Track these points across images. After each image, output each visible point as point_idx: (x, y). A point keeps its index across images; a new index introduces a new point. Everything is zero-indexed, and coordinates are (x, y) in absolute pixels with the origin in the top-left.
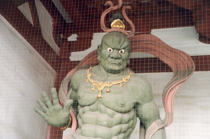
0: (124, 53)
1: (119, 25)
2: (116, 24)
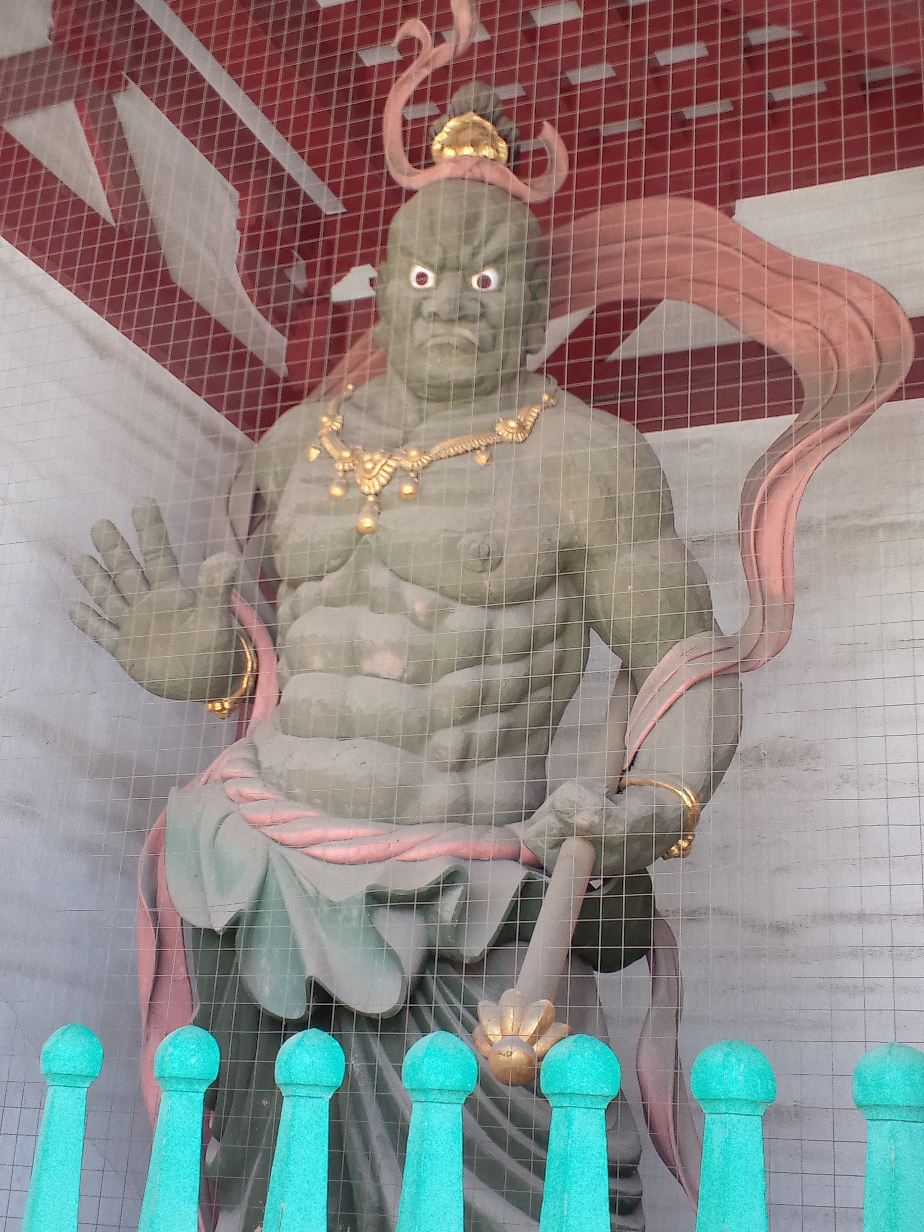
0: (499, 290)
1: (475, 144)
2: (454, 143)
